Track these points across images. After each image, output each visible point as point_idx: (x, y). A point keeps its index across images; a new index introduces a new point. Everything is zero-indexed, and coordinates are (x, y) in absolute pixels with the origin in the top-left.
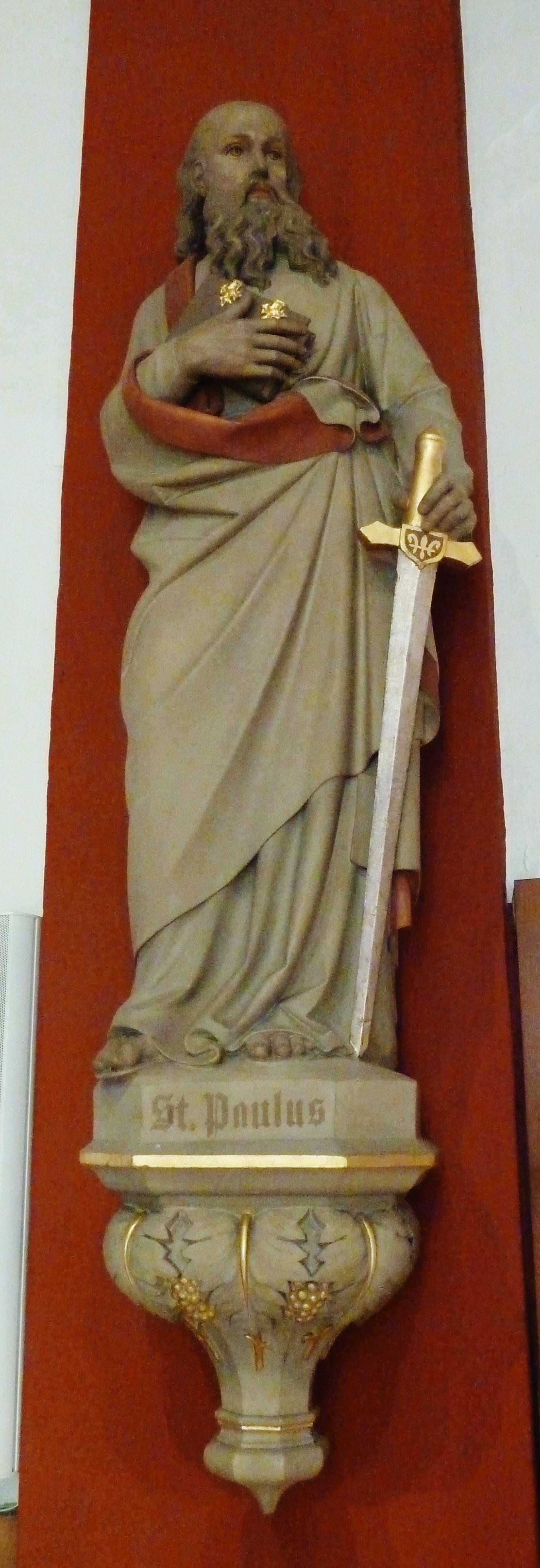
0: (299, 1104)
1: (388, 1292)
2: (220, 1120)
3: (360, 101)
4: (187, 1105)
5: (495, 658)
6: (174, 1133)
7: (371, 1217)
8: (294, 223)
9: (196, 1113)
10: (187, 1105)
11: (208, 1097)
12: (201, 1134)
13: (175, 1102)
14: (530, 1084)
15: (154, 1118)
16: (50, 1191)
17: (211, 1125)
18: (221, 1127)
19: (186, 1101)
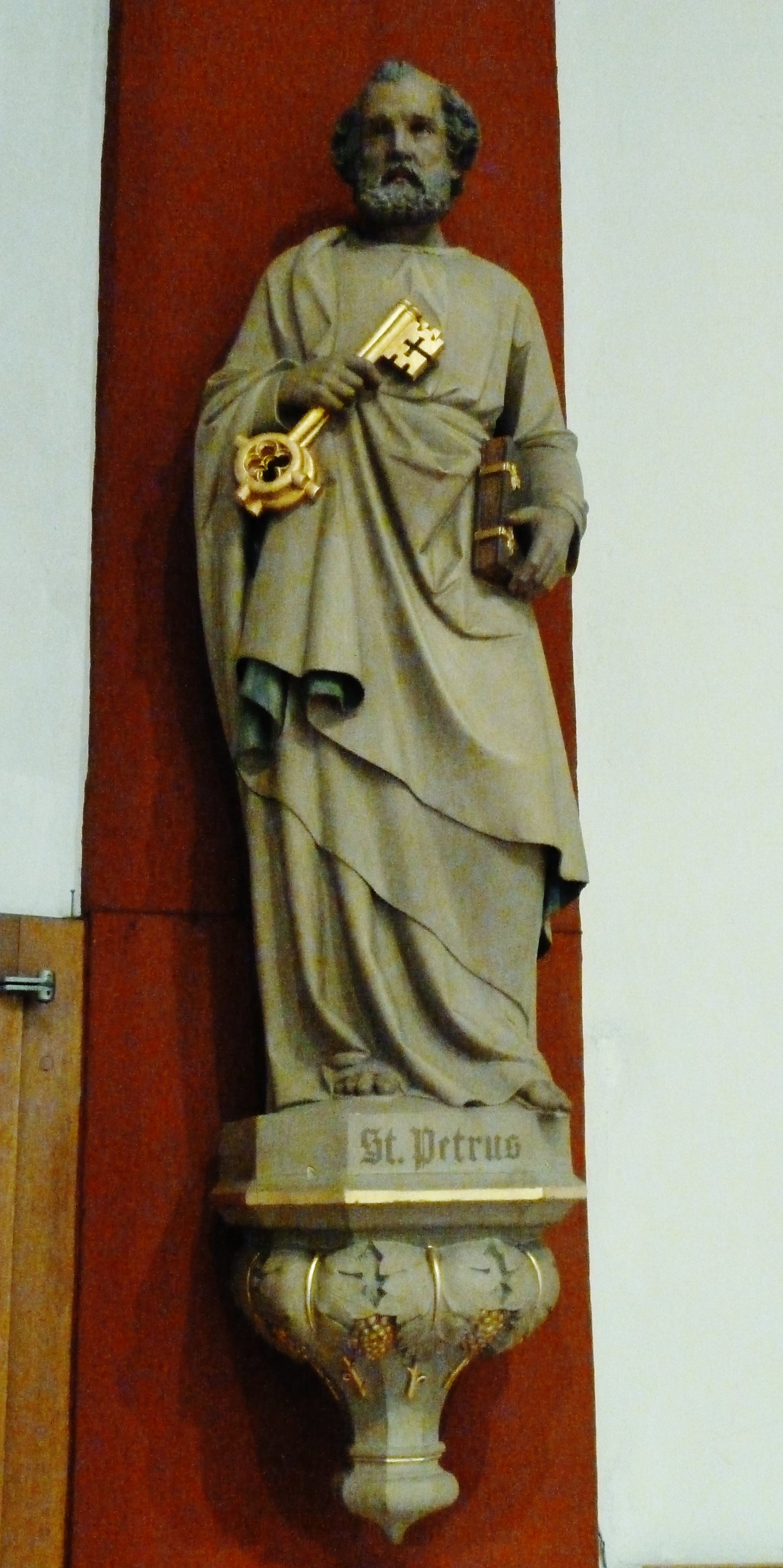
0: (498, 1138)
1: (248, 843)
2: (427, 1154)
3: (379, 148)
4: (395, 1138)
5: (576, 748)
6: (383, 1168)
7: (391, 1135)
8: (431, 731)
9: (404, 1146)
10: (395, 1138)
11: (416, 1133)
12: (409, 1166)
13: (382, 1136)
14: (56, 1498)
15: (363, 1151)
16: (32, 1249)
17: (420, 1160)
18: (428, 1161)
19: (394, 1134)
